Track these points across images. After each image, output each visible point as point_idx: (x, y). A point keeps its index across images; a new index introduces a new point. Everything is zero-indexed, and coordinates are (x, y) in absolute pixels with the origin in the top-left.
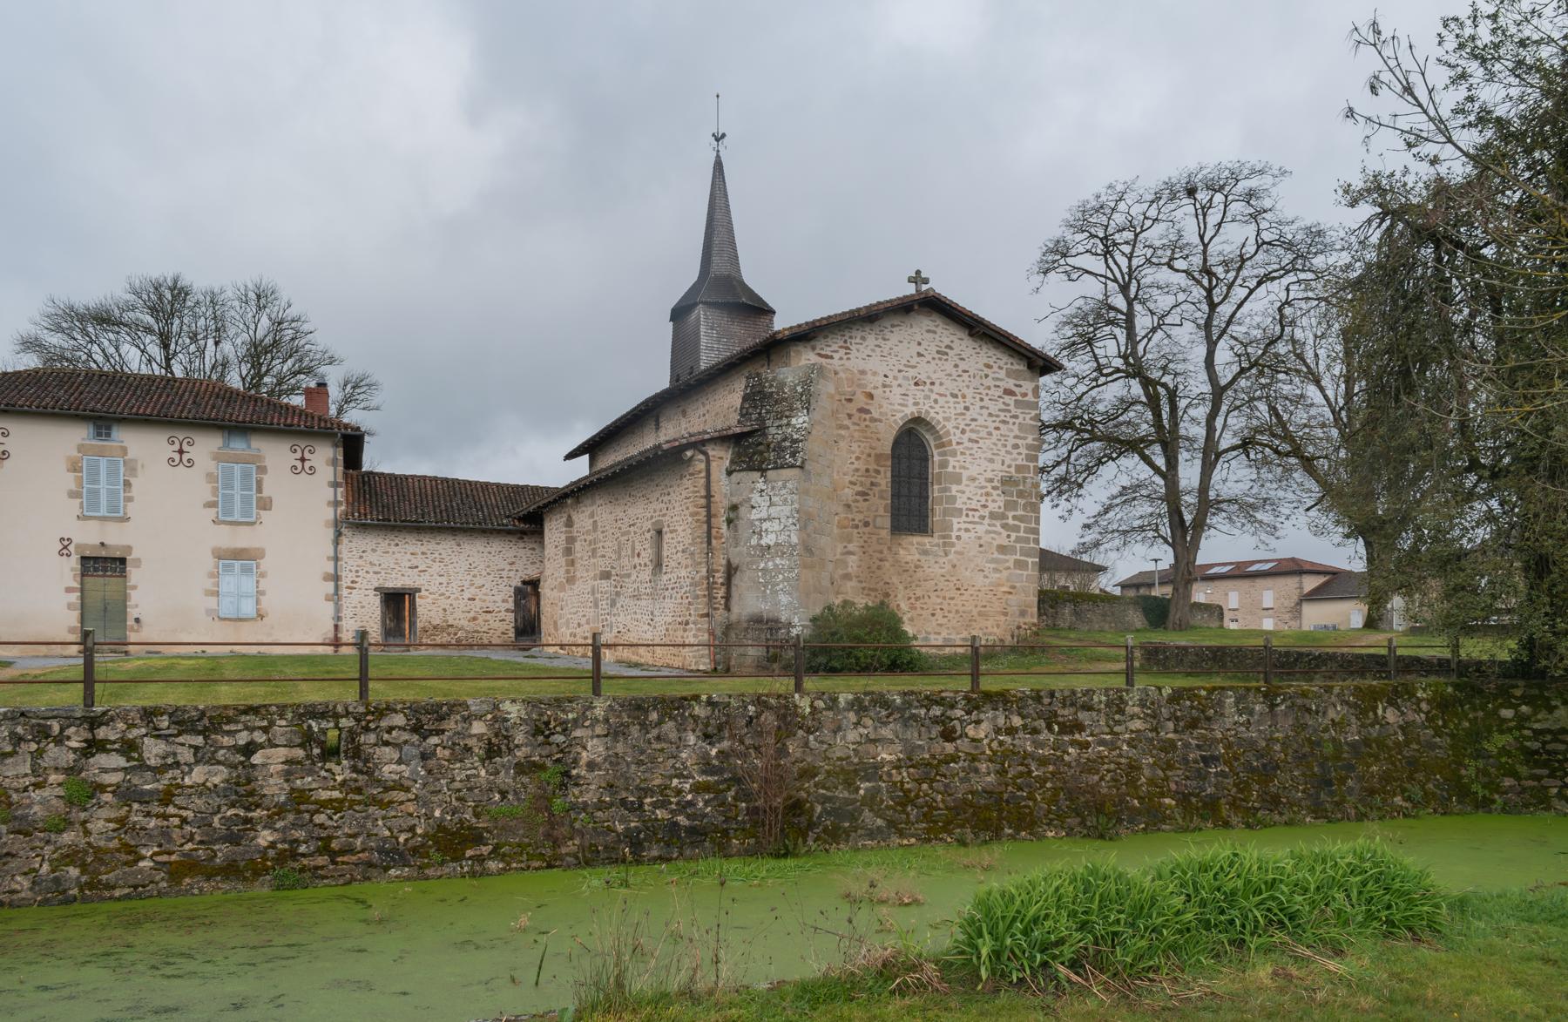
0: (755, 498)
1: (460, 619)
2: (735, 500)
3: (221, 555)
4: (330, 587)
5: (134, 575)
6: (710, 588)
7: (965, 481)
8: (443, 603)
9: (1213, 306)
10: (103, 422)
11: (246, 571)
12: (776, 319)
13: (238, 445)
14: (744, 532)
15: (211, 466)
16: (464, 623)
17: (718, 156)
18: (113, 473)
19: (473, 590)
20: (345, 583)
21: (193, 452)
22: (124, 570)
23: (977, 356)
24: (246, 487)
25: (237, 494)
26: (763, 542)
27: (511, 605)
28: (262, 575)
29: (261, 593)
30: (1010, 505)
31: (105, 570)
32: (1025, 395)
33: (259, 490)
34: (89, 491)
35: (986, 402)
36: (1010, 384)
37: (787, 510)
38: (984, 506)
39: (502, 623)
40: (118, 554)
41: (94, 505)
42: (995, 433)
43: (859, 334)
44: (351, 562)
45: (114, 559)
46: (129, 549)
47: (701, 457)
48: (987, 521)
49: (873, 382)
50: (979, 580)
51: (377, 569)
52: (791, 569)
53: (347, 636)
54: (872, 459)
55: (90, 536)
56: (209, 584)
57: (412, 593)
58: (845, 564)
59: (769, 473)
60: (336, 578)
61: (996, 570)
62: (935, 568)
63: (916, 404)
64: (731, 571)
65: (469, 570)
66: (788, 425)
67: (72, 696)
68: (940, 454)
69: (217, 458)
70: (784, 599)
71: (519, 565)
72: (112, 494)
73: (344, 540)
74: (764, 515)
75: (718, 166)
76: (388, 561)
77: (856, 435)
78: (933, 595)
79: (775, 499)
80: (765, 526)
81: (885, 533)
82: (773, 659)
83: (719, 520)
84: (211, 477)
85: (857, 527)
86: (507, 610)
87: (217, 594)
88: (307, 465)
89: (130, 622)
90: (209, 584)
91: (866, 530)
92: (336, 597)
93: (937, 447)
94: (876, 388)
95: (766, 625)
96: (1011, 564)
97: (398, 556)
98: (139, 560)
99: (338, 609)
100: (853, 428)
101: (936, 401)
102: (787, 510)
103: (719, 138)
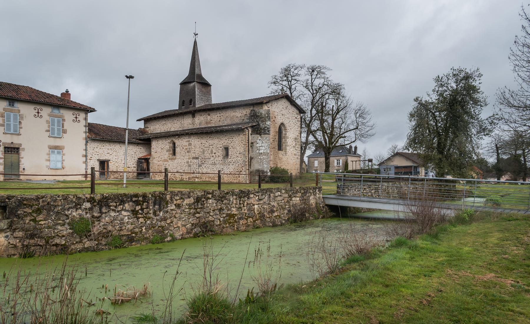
0: (258, 141)
2: (252, 141)
3: (51, 148)
5: (22, 154)
8: (117, 164)
10: (12, 100)
11: (59, 153)
13: (56, 111)
14: (255, 149)
15: (48, 118)
18: (15, 119)
20: (89, 158)
21: (42, 113)
22: (18, 152)
24: (59, 126)
25: (56, 128)
27: (135, 165)
28: (64, 155)
29: (63, 160)
30: (296, 144)
31: (11, 151)
33: (63, 127)
34: (7, 124)
36: (296, 116)
37: (267, 144)
40: (17, 146)
41: (9, 129)
45: (14, 148)
46: (21, 145)
49: (276, 114)
50: (291, 162)
52: (267, 159)
55: (8, 140)
56: (47, 157)
60: (86, 156)
62: (284, 159)
64: (251, 159)
67: (87, 193)
69: (50, 115)
70: (265, 166)
71: (137, 153)
72: (15, 126)
74: (260, 145)
75: (195, 43)
76: (101, 151)
81: (277, 150)
84: (48, 122)
87: (49, 160)
88: (40, 115)
89: (21, 170)
90: (47, 157)
92: (86, 162)
98: (24, 149)
102: (267, 144)
103: (196, 35)
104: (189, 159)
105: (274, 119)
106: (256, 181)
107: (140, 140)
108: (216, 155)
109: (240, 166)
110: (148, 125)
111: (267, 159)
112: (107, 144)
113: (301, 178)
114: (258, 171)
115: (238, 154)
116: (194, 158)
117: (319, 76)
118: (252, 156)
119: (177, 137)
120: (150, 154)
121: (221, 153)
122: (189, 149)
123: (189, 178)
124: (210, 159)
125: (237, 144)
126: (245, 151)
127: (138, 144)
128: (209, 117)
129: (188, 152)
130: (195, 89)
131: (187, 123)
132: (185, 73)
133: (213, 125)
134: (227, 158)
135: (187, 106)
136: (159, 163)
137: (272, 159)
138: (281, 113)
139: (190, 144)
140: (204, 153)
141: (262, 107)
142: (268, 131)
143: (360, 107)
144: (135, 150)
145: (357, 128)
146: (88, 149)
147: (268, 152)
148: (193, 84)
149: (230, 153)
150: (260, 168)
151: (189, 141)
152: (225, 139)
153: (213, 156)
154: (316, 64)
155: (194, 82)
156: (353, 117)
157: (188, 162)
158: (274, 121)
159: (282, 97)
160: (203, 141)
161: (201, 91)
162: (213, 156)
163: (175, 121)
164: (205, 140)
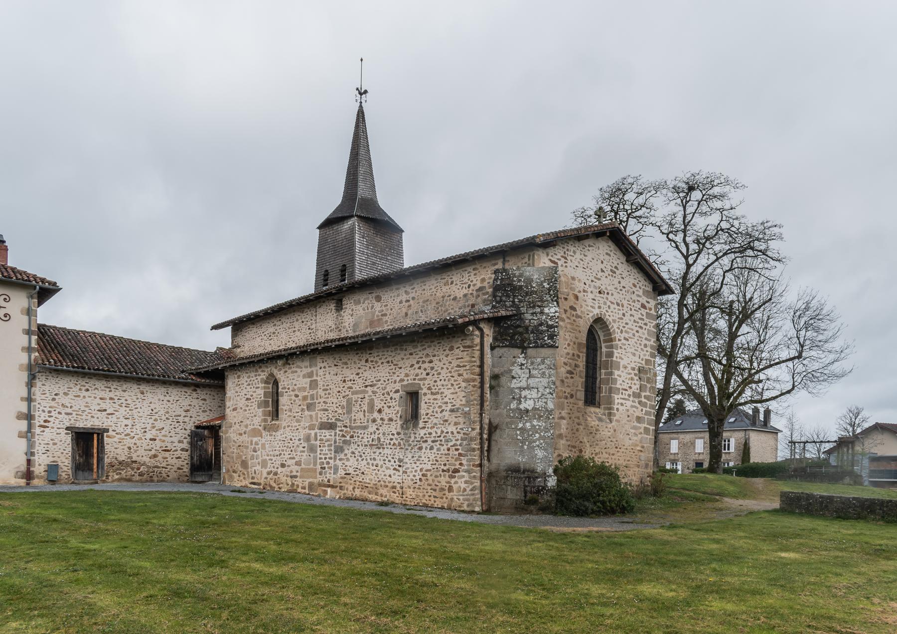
0: (516, 370)
1: (142, 455)
2: (497, 371)
4: (23, 425)
6: (481, 439)
7: (621, 369)
8: (129, 442)
9: (689, 266)
12: (407, 240)
14: (504, 397)
17: (361, 106)
19: (154, 432)
20: (38, 421)
23: (631, 278)
26: (522, 407)
27: (186, 445)
32: (650, 309)
35: (633, 312)
36: (644, 300)
37: (544, 381)
38: (630, 387)
39: (178, 458)
42: (637, 334)
43: (572, 249)
44: (44, 403)
47: (477, 333)
48: (631, 398)
49: (579, 286)
50: (628, 442)
51: (69, 410)
52: (546, 430)
53: (39, 469)
54: (575, 346)
57: (101, 433)
58: (560, 426)
59: (530, 351)
60: (29, 417)
61: (635, 434)
62: (606, 431)
63: (599, 307)
64: (493, 428)
65: (151, 415)
66: (542, 313)
68: (607, 347)
70: (540, 454)
71: (193, 412)
73: (38, 383)
74: (523, 384)
75: (361, 115)
76: (79, 404)
77: (569, 326)
78: (604, 451)
79: (534, 372)
80: (524, 393)
81: (581, 403)
82: (533, 502)
83: (489, 385)
85: (566, 398)
86: (182, 450)
91: (572, 400)
92: (28, 435)
93: (605, 341)
94: (580, 292)
95: (523, 475)
96: (642, 430)
97: (88, 399)
99: (31, 445)
100: (567, 321)
101: (609, 307)
102: (544, 381)
104: (311, 427)
105: (571, 301)
106: (507, 503)
107: (199, 375)
108: (384, 415)
109: (453, 452)
110: (240, 340)
111: (546, 430)
112: (100, 384)
113: (656, 492)
114: (515, 470)
115: (447, 414)
117: (704, 208)
118: (496, 421)
119: (280, 363)
120: (223, 417)
121: (395, 409)
124: (365, 428)
125: (446, 380)
126: (468, 403)
128: (378, 306)
130: (353, 237)
131: (323, 325)
132: (332, 199)
134: (416, 425)
135: (336, 286)
136: (241, 438)
137: (563, 430)
138: (594, 282)
139: (314, 385)
140: (349, 412)
141: (532, 258)
142: (551, 337)
143: (808, 303)
145: (799, 357)
147: (551, 406)
149: (423, 409)
150: (521, 460)
151: (310, 375)
152: (408, 363)
153: (374, 421)
154: (703, 166)
156: (788, 328)
157: (308, 439)
158: (573, 308)
159: (599, 234)
160: (349, 374)
161: (370, 243)
162: (374, 421)
164: (355, 371)
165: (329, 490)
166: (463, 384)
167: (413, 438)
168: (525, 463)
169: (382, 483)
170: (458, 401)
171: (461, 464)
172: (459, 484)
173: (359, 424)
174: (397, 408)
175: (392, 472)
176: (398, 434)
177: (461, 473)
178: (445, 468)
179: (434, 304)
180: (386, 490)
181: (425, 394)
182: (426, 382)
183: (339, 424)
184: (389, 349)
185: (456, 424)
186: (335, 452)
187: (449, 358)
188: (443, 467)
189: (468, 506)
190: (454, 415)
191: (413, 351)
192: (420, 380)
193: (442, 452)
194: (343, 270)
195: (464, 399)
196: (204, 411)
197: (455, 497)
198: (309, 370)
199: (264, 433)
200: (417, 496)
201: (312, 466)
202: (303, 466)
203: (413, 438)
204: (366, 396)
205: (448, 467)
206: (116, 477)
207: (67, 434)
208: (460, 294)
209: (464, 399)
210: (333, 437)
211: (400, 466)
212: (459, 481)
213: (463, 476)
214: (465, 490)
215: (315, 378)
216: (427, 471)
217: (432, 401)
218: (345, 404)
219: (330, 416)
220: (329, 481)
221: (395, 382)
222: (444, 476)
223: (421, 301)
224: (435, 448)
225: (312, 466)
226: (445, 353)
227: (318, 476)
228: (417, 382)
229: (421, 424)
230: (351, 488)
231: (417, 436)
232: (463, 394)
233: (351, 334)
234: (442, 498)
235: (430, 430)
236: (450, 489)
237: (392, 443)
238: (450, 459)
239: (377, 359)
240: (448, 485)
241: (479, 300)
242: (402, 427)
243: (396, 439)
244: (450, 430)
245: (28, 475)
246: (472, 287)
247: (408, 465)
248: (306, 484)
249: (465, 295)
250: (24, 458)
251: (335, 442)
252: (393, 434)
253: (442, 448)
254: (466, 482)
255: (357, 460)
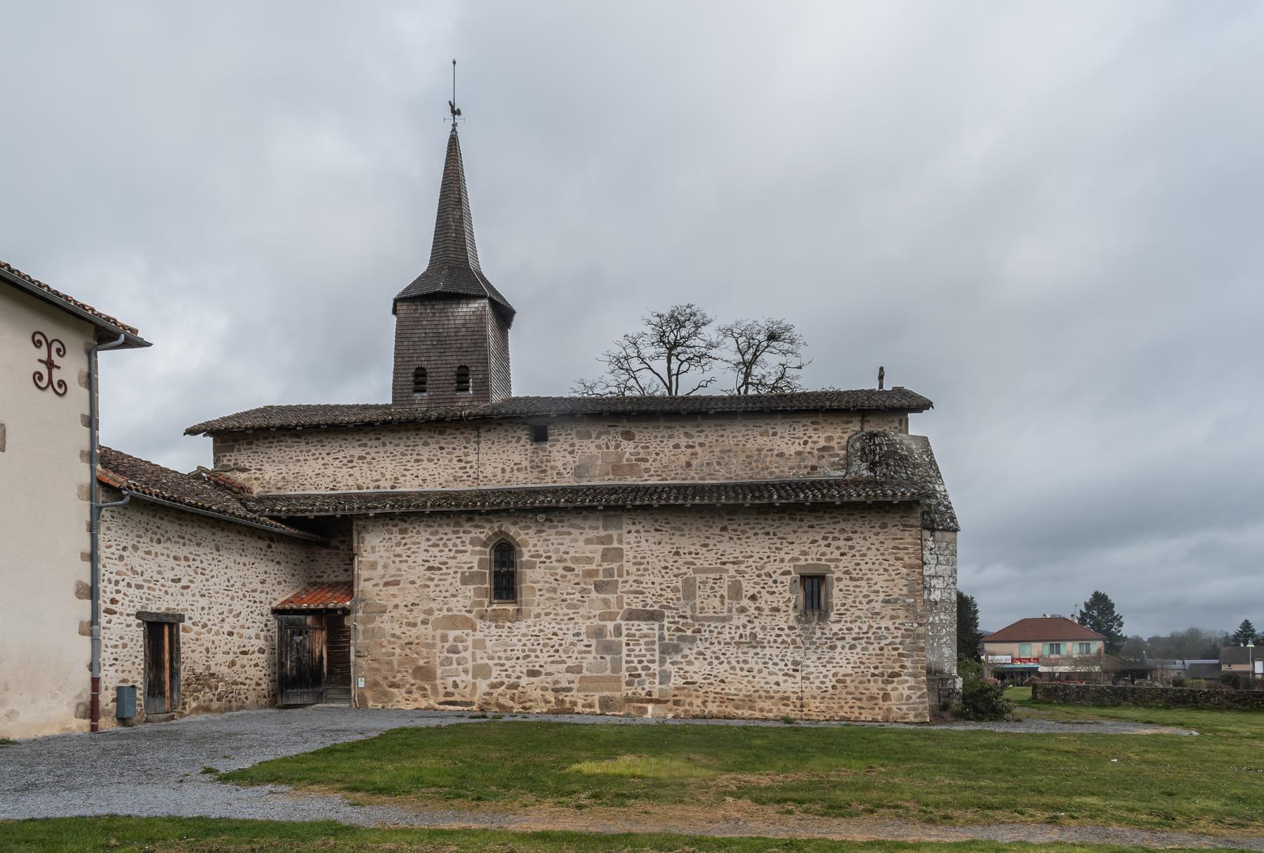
16: (224, 669)
17: (454, 130)
26: (931, 598)
59: (938, 534)
60: (92, 593)
74: (932, 572)
75: (453, 143)
80: (934, 582)
108: (761, 603)
116: (632, 615)
121: (787, 596)
122: (609, 572)
123: (606, 704)
127: (270, 537)
128: (628, 447)
129: (599, 587)
130: (483, 328)
132: (412, 260)
133: (654, 481)
134: (824, 616)
136: (413, 631)
139: (614, 555)
144: (261, 570)
146: (103, 552)
148: (475, 305)
152: (812, 535)
153: (743, 610)
155: (450, 304)
162: (743, 610)
163: (425, 452)
165: (650, 707)
166: (905, 571)
167: (818, 634)
168: (936, 663)
169: (763, 694)
170: (896, 589)
171: (902, 667)
172: (901, 690)
173: (711, 614)
174: (788, 595)
175: (781, 678)
176: (791, 628)
177: (903, 678)
178: (877, 672)
179: (742, 457)
180: (769, 702)
181: (839, 579)
182: (841, 564)
183: (667, 613)
184: (769, 517)
185: (892, 618)
186: (662, 652)
187: (881, 537)
188: (872, 670)
189: (916, 716)
190: (890, 607)
191: (815, 523)
192: (830, 560)
193: (871, 651)
194: (462, 378)
195: (905, 589)
196: (279, 583)
197: (894, 708)
198: (602, 533)
199: (479, 624)
200: (829, 708)
201: (608, 673)
202: (585, 673)
203: (818, 634)
204: (725, 576)
205: (881, 670)
206: (194, 705)
207: (138, 626)
208: (791, 450)
209: (905, 589)
210: (657, 632)
211: (795, 670)
212: (900, 687)
213: (907, 681)
214: (909, 697)
215: (615, 545)
216: (845, 675)
217: (852, 589)
218: (680, 585)
219: (650, 602)
220: (649, 694)
221: (782, 561)
222: (875, 681)
223: (717, 450)
224: (859, 647)
225: (608, 673)
226: (874, 530)
227: (624, 687)
228: (823, 562)
229: (833, 617)
230: (699, 702)
231: (826, 631)
232: (905, 582)
233: (568, 481)
234: (873, 709)
235: (849, 625)
236: (886, 697)
237: (780, 640)
238: (884, 660)
239: (747, 528)
240: (881, 693)
241: (824, 462)
242: (798, 620)
243: (788, 636)
244: (883, 625)
245: (93, 711)
246: (810, 444)
247: (812, 669)
248: (596, 698)
249: (799, 453)
250: (87, 676)
251: (661, 638)
252: (782, 629)
253: (871, 647)
254: (909, 688)
255: (711, 663)
